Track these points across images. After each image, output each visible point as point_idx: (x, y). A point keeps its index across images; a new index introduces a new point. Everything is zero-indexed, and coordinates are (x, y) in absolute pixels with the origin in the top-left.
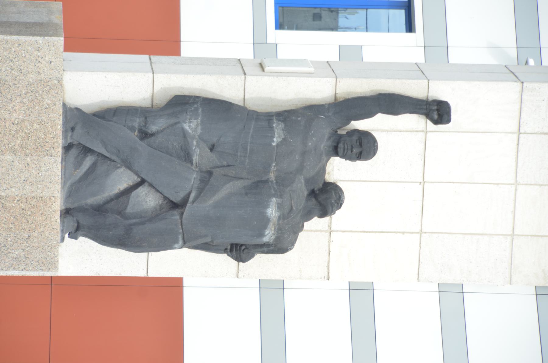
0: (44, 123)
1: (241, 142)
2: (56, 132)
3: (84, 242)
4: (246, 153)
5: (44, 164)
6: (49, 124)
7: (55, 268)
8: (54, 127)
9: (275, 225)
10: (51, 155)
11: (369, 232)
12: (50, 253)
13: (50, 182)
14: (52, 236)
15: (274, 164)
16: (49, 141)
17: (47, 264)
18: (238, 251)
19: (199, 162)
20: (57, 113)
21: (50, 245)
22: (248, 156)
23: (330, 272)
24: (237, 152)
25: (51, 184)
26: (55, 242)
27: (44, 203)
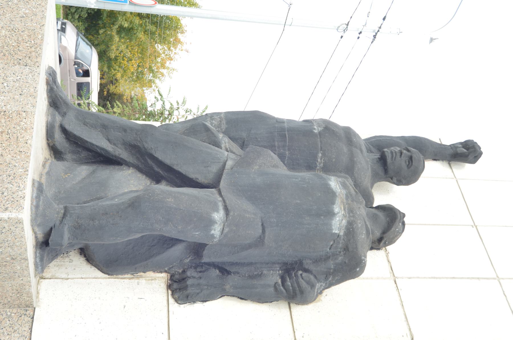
0: (17, 31)
1: (276, 131)
2: (34, 42)
3: (76, 299)
4: (285, 141)
5: (14, 74)
6: (26, 32)
7: (18, 207)
8: (32, 36)
9: (344, 203)
10: (25, 64)
11: (440, 278)
12: (11, 186)
13: (20, 94)
14: (18, 161)
15: (320, 155)
16: (23, 49)
17: (4, 202)
18: (294, 278)
19: (229, 148)
20: (38, 23)
21: (13, 174)
22: (287, 145)
23: (411, 328)
24: (274, 141)
25: (22, 96)
26: (21, 170)
27: (8, 118)
